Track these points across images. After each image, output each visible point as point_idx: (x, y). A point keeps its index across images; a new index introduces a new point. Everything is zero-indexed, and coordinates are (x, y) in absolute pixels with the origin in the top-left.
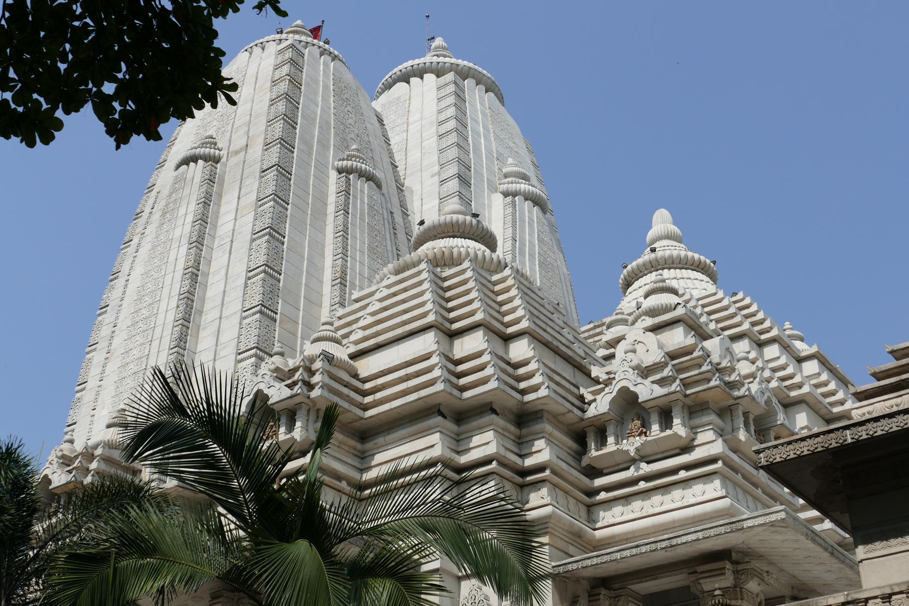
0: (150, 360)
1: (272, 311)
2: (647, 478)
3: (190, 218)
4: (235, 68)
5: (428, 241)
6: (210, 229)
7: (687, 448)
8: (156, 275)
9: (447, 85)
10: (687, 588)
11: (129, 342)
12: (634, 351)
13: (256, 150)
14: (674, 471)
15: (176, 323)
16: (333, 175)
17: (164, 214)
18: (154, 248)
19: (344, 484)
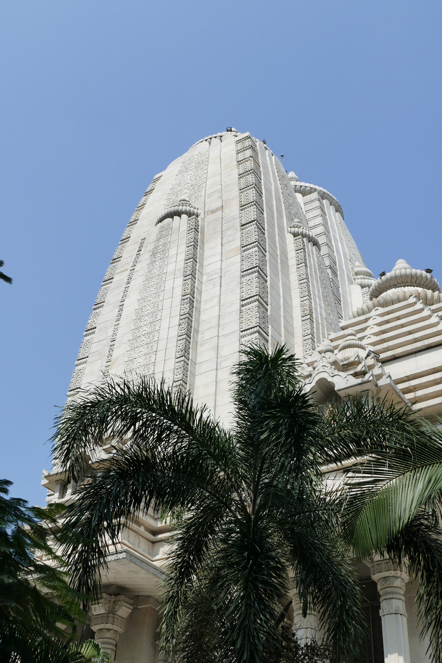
0: (156, 367)
1: (266, 333)
3: (182, 257)
4: (196, 152)
5: (390, 287)
6: (199, 266)
8: (154, 300)
9: (312, 201)
13: (233, 209)
15: (179, 338)
16: (290, 238)
17: (154, 254)
18: (148, 279)
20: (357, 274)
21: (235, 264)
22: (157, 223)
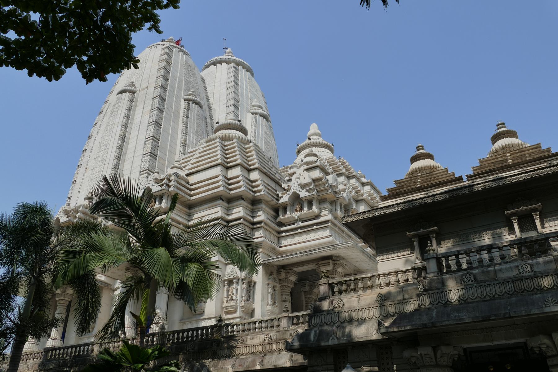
2: (301, 228)
13: (151, 89)
19: (181, 226)
20: (253, 106)
21: (146, 119)
22: (118, 94)
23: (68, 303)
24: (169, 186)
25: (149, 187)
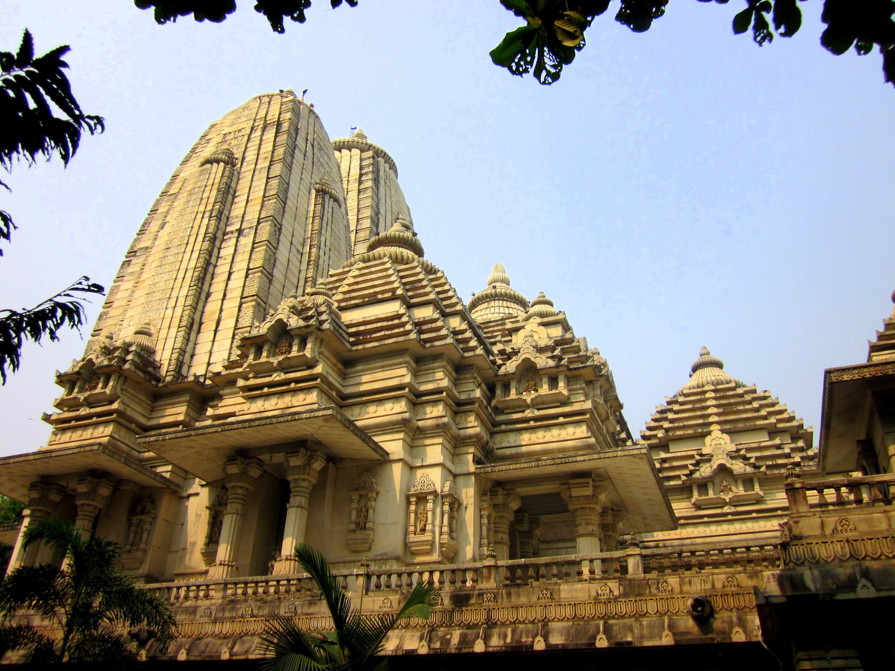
2: (536, 419)
7: (564, 404)
10: (558, 494)
11: (156, 277)
12: (532, 336)
14: (556, 416)
19: (334, 393)
23: (97, 512)
24: (125, 361)
25: (91, 360)
